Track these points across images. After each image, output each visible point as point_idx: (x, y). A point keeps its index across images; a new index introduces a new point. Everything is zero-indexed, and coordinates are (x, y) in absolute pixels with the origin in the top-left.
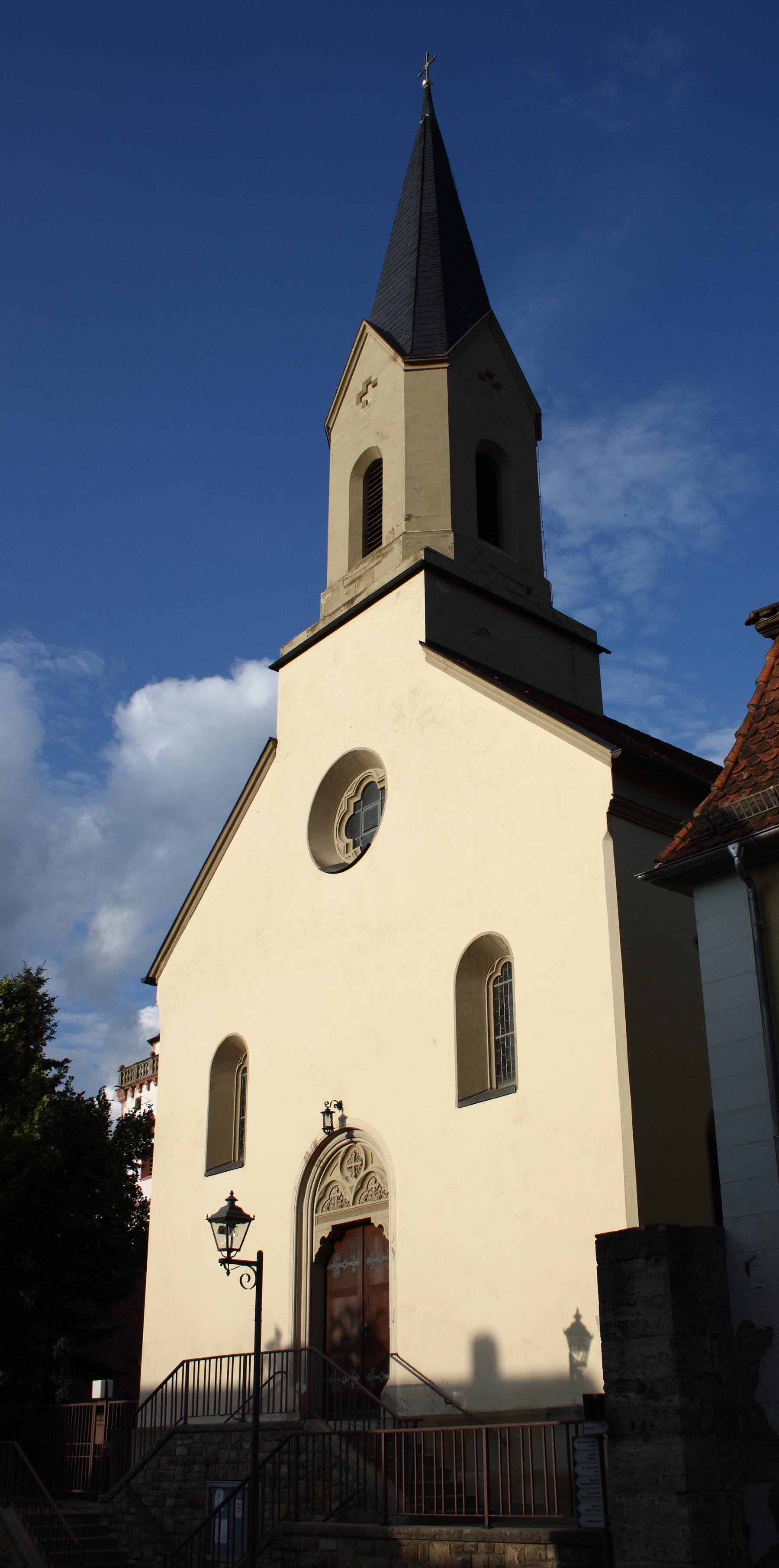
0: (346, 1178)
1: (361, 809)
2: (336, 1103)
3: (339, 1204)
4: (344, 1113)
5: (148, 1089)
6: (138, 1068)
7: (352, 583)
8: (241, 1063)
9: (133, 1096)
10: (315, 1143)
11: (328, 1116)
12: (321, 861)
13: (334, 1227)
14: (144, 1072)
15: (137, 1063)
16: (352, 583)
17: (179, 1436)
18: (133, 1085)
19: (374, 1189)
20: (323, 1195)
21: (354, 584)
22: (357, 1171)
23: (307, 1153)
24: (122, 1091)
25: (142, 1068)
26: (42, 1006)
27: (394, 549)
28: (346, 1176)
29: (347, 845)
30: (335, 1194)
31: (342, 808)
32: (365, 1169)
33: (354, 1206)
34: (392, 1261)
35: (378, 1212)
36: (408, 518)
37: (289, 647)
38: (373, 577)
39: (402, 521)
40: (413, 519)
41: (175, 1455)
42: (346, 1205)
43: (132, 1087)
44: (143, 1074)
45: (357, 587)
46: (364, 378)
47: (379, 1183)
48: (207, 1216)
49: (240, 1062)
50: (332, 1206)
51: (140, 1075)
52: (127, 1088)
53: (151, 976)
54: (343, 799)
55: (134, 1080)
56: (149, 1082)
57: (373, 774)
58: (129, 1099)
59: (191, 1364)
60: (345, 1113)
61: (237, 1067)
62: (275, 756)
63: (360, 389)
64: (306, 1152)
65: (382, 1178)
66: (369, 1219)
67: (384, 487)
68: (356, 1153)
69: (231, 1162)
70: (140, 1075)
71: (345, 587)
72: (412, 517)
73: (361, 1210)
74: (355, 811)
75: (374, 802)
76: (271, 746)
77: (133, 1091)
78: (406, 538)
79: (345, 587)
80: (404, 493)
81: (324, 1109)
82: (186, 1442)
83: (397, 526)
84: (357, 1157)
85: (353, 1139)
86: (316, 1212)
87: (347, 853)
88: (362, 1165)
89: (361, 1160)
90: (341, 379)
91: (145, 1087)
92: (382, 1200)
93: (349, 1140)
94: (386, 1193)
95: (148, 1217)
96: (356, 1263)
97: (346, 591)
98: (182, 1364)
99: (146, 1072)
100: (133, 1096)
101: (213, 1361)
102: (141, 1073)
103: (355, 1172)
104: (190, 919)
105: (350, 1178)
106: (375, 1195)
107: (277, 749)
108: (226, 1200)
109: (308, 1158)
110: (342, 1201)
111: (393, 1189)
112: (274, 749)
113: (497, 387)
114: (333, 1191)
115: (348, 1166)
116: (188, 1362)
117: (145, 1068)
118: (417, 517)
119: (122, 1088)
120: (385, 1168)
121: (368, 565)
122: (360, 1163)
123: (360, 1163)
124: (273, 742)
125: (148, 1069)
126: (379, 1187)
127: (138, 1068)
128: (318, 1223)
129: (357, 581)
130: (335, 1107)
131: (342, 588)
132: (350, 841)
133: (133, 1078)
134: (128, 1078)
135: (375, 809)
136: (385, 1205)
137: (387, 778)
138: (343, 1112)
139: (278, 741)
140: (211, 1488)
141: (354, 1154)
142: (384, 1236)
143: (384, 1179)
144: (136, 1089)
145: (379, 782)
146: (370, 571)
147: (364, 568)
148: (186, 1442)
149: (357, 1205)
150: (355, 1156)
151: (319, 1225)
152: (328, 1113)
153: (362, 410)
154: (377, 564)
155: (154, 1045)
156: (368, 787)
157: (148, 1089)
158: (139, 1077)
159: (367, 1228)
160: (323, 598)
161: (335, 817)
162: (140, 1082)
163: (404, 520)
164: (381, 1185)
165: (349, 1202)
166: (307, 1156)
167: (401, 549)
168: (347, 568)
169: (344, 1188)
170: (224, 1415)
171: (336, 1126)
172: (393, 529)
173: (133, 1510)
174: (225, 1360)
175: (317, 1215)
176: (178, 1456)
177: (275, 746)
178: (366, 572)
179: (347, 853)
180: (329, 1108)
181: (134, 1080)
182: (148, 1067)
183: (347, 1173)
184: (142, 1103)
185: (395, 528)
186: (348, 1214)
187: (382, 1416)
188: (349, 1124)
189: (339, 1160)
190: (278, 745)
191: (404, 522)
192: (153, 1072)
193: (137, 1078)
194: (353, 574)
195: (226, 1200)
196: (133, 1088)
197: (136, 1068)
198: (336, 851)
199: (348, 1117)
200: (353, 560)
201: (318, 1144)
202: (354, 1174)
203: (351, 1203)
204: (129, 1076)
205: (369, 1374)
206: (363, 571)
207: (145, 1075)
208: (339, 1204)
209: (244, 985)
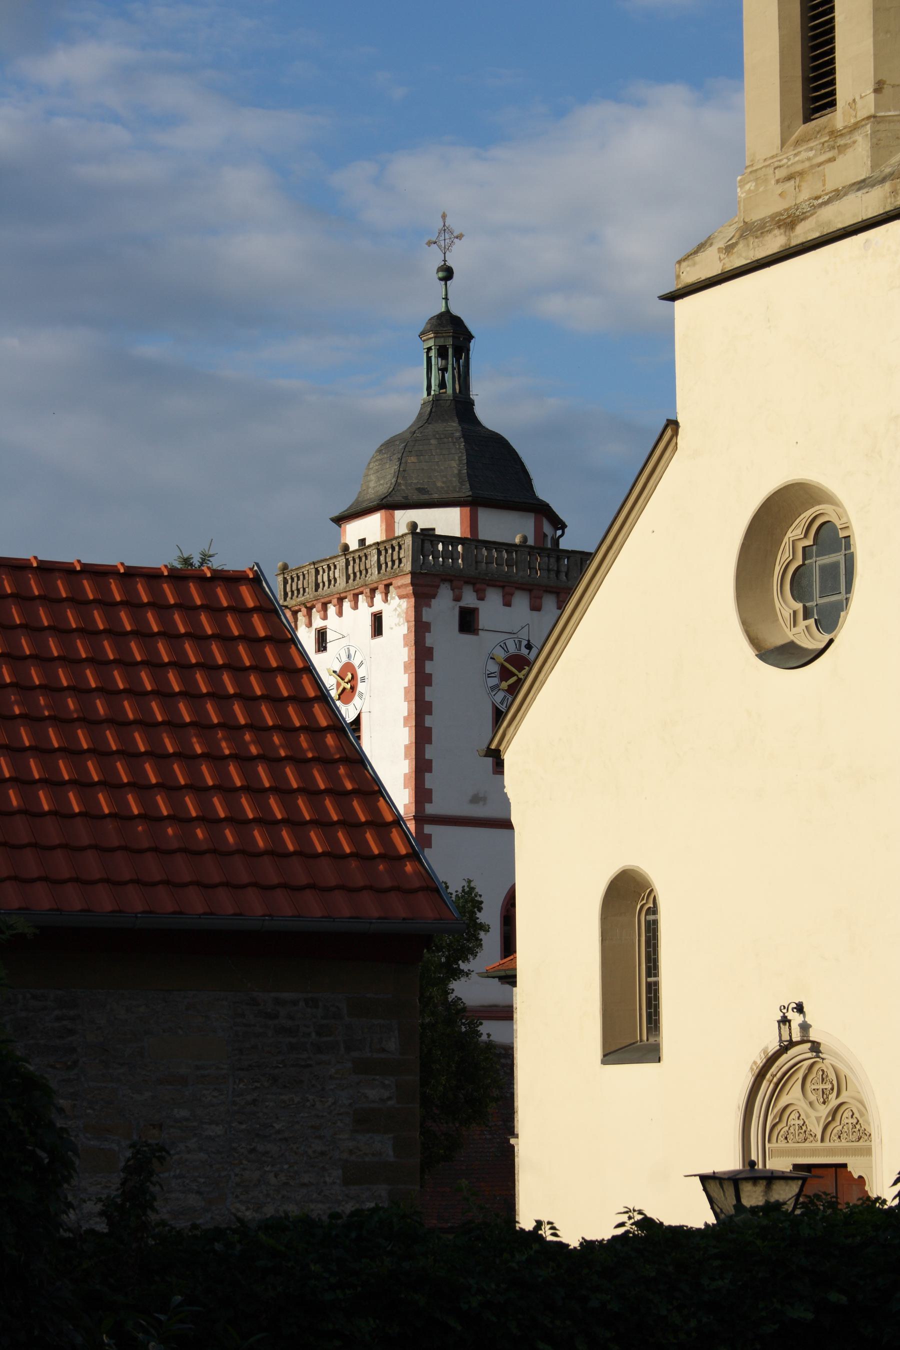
0: (811, 1104)
1: (814, 559)
2: (795, 1006)
3: (801, 1135)
4: (806, 1020)
5: (340, 613)
6: (317, 572)
7: (789, 178)
8: (644, 901)
9: (310, 624)
10: (765, 1051)
11: (785, 1024)
12: (757, 639)
14: (330, 581)
15: (314, 563)
16: (789, 178)
18: (308, 605)
19: (851, 1126)
20: (777, 1120)
21: (792, 182)
22: (825, 1096)
23: (755, 1063)
25: (324, 572)
26: (192, 567)
27: (856, 144)
28: (811, 1100)
29: (795, 612)
30: (794, 1121)
31: (784, 555)
33: (823, 1144)
35: (856, 1158)
36: (879, 88)
37: (688, 266)
38: (824, 181)
39: (868, 92)
40: (887, 90)
42: (812, 1139)
43: (306, 607)
44: (327, 584)
45: (797, 189)
47: (856, 1118)
49: (643, 899)
50: (792, 1137)
51: (321, 585)
52: (296, 608)
53: (493, 747)
54: (786, 539)
55: (310, 594)
56: (341, 600)
57: (829, 513)
60: (809, 1020)
61: (639, 907)
64: (752, 1062)
65: (862, 1115)
67: (839, 54)
68: (823, 1071)
69: (637, 1042)
70: (321, 585)
71: (778, 181)
72: (885, 86)
73: (831, 1152)
74: (804, 558)
75: (834, 553)
76: (669, 433)
77: (309, 615)
78: (876, 129)
79: (778, 181)
80: (871, 40)
81: (779, 1016)
83: (861, 97)
84: (824, 1076)
85: (820, 1054)
86: (769, 1141)
87: (794, 626)
88: (832, 1089)
89: (831, 1083)
90: (845, 545)
91: (332, 610)
92: (861, 1143)
93: (814, 1054)
94: (868, 1134)
95: (603, 1240)
97: (779, 189)
99: (332, 581)
100: (310, 624)
102: (324, 583)
103: (823, 1097)
104: (550, 673)
105: (816, 1104)
106: (852, 1134)
107: (679, 437)
110: (805, 1132)
111: (878, 1138)
112: (675, 437)
114: (792, 1116)
115: (814, 1087)
117: (331, 572)
118: (893, 86)
120: (865, 1100)
121: (815, 156)
122: (829, 1086)
123: (830, 1086)
124: (673, 425)
125: (337, 575)
126: (857, 1124)
127: (317, 572)
128: (771, 1157)
129: (798, 179)
130: (793, 1011)
131: (773, 182)
132: (799, 606)
133: (307, 589)
134: (298, 590)
135: (840, 602)
136: (868, 1152)
137: (854, 534)
138: (804, 1017)
139: (680, 424)
141: (821, 1073)
142: (867, 1191)
143: (864, 1115)
144: (314, 610)
145: (840, 529)
146: (818, 169)
147: (809, 159)
149: (827, 1144)
150: (822, 1075)
151: (773, 1159)
152: (784, 1021)
155: (342, 526)
156: (824, 526)
157: (340, 613)
158: (320, 589)
159: (842, 1169)
160: (741, 187)
161: (775, 565)
162: (323, 600)
163: (872, 90)
164: (860, 1122)
165: (815, 1136)
167: (868, 148)
168: (779, 142)
169: (808, 1116)
171: (796, 1037)
172: (854, 100)
175: (771, 1145)
177: (676, 433)
178: (812, 167)
179: (794, 626)
180: (786, 1015)
181: (310, 594)
182: (337, 571)
183: (812, 1097)
184: (329, 638)
186: (814, 1152)
188: (813, 1035)
189: (800, 1075)
190: (680, 430)
191: (873, 95)
192: (347, 582)
193: (316, 590)
194: (790, 163)
196: (309, 610)
197: (313, 571)
198: (778, 620)
199: (813, 1027)
200: (789, 127)
201: (770, 1054)
202: (822, 1100)
203: (819, 1136)
204: (300, 586)
206: (807, 164)
207: (332, 586)
208: (801, 1135)
209: (646, 798)
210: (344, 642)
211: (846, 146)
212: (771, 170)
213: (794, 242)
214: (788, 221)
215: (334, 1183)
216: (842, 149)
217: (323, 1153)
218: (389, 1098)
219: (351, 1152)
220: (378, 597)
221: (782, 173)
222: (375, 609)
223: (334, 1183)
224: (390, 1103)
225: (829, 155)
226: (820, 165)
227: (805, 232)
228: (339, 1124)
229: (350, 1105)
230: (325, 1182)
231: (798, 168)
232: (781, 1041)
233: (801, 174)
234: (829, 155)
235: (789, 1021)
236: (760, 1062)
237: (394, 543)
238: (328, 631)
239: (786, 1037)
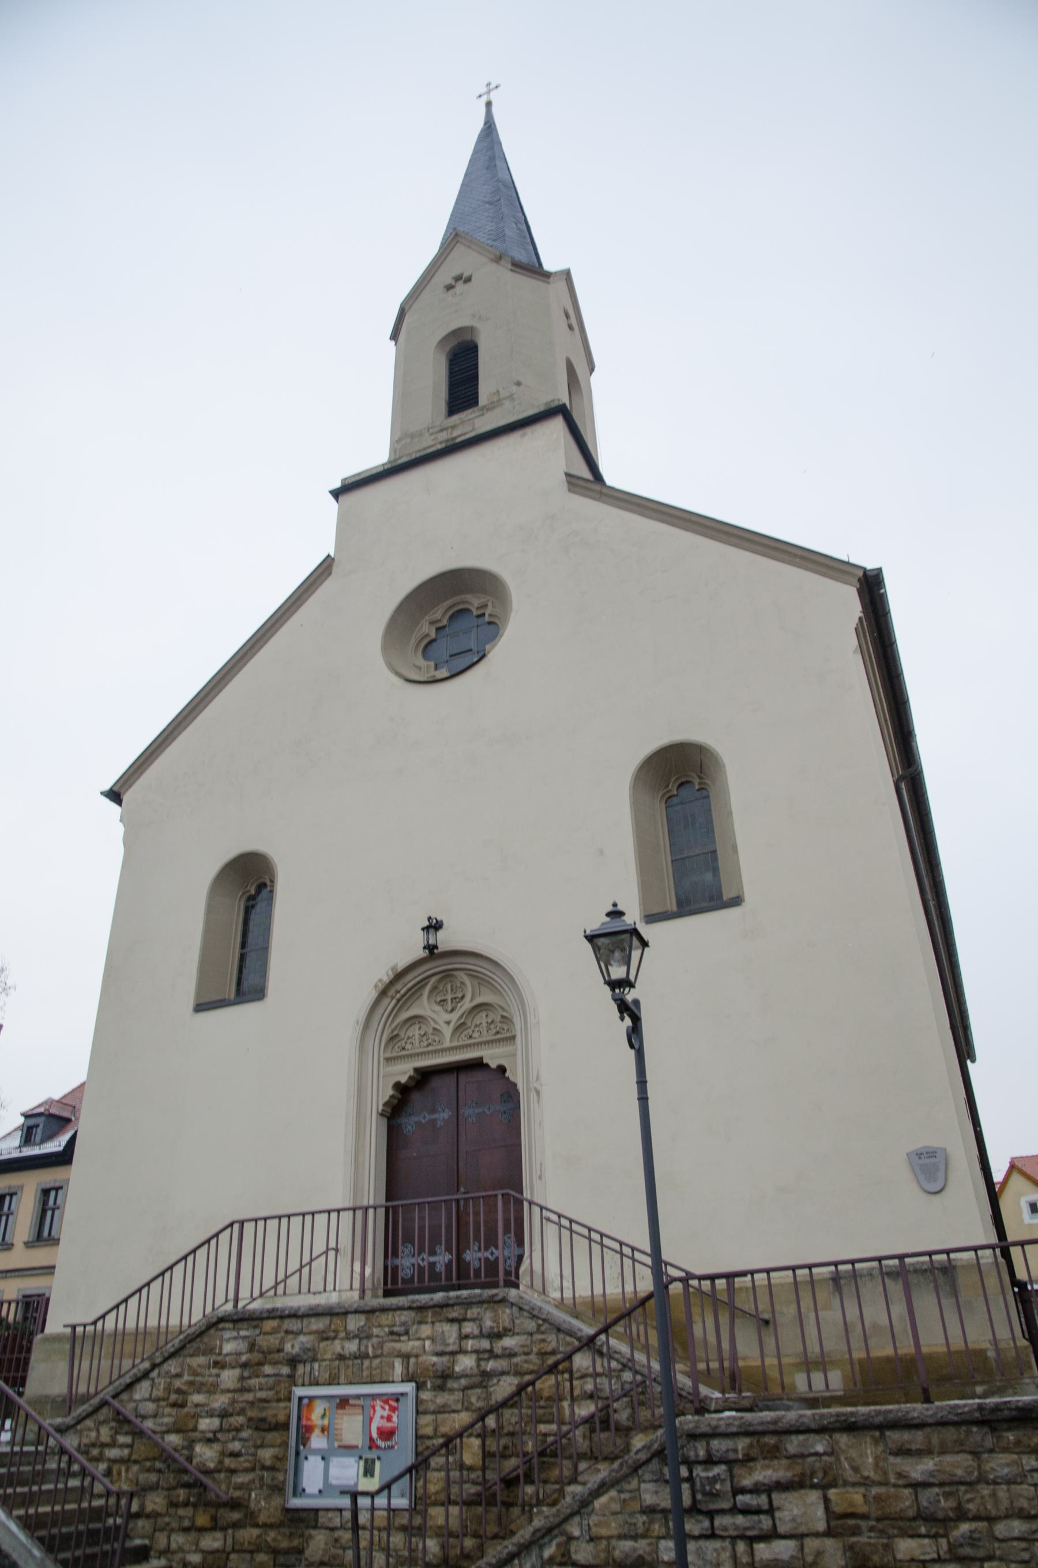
13: (416, 1070)
17: (230, 1325)
23: (380, 980)
32: (472, 1000)
34: (536, 1105)
41: (220, 1354)
46: (456, 272)
48: (585, 932)
59: (249, 1227)
63: (450, 281)
66: (481, 1058)
82: (243, 1333)
96: (444, 1115)
98: (231, 1225)
101: (273, 1224)
108: (22, 1114)
109: (381, 986)
116: (242, 1223)
140: (300, 1399)
148: (243, 1333)
154: (478, 416)
166: (380, 985)
170: (320, 1293)
173: (122, 1439)
174: (296, 1221)
176: (227, 1355)
185: (501, 390)
195: (22, 1114)
205: (468, 1251)
236: (386, 980)
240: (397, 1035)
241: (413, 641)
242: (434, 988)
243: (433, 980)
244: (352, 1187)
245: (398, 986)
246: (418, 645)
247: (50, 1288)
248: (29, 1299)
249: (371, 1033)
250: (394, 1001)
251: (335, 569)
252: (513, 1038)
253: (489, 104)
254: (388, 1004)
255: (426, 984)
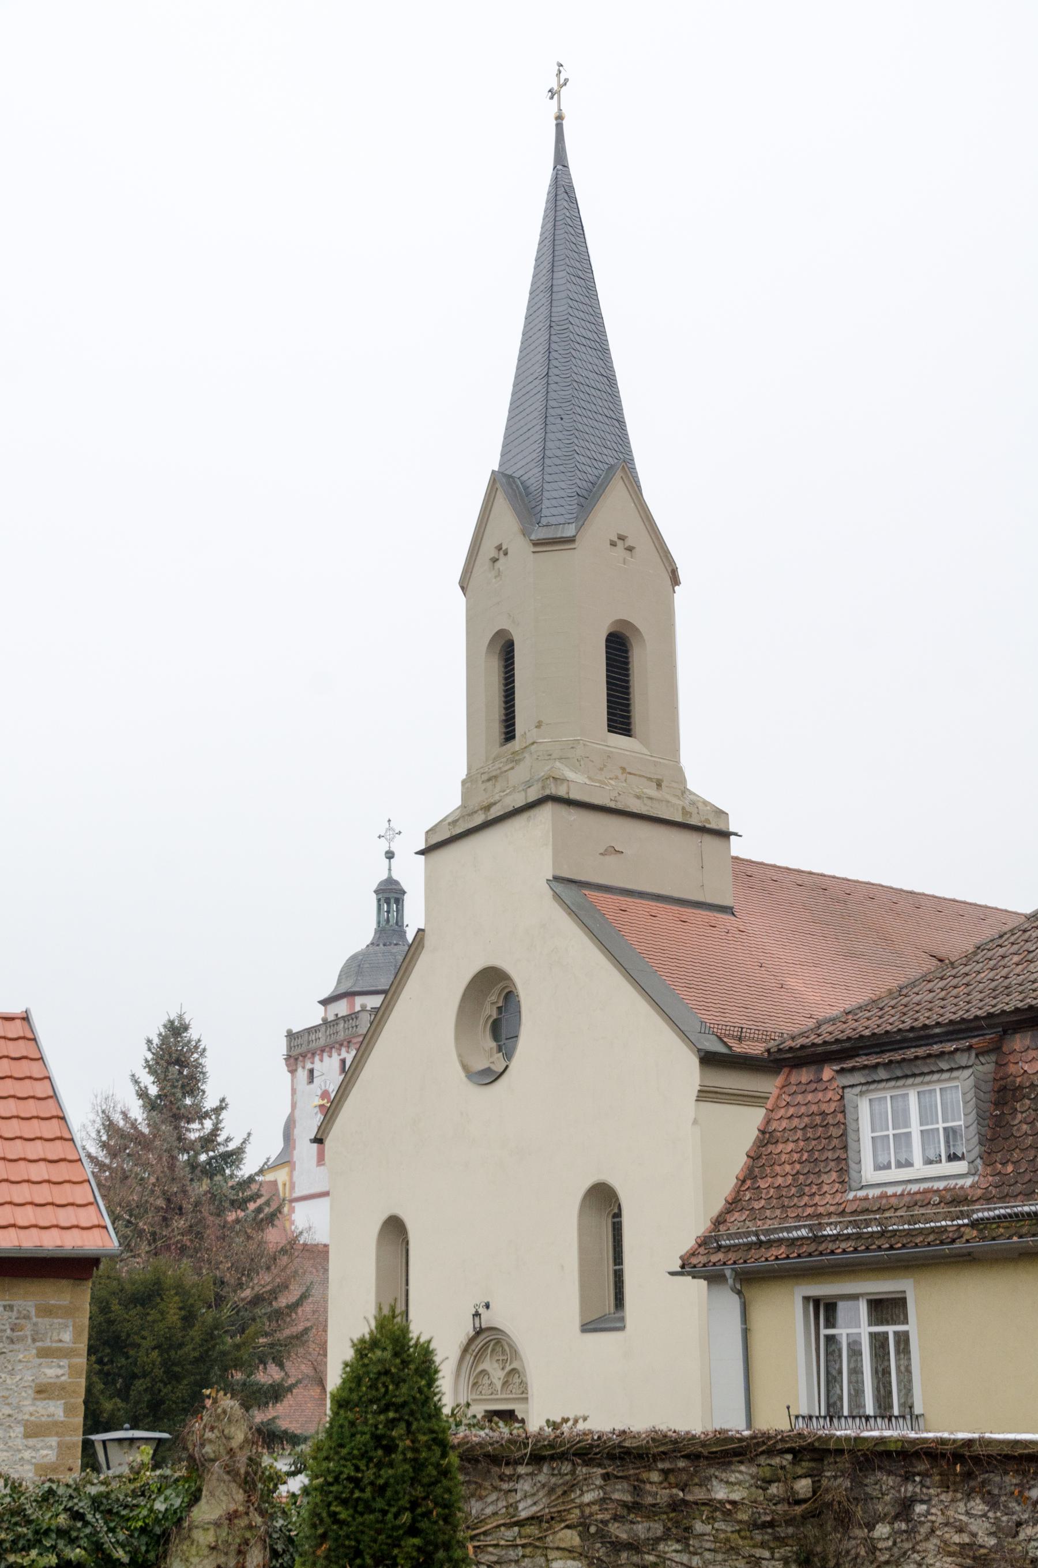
5: (321, 1060)
7: (489, 780)
9: (304, 1068)
13: (486, 1411)
16: (489, 780)
24: (292, 1060)
58: (300, 1070)
62: (423, 947)
71: (483, 782)
79: (483, 782)
100: (304, 1068)
109: (462, 1348)
113: (630, 549)
119: (290, 1056)
147: (500, 768)
152: (477, 1314)
153: (494, 580)
157: (321, 1060)
178: (502, 773)
187: (1025, 1203)
206: (498, 771)
210: (323, 1077)
211: (520, 760)
212: (479, 775)
213: (489, 818)
214: (487, 808)
215: (17, 1437)
216: (518, 762)
217: (9, 1416)
218: (63, 1375)
219: (31, 1414)
220: (344, 1050)
221: (485, 777)
222: (342, 1057)
223: (17, 1437)
224: (63, 1378)
225: (511, 765)
226: (506, 771)
227: (495, 812)
228: (24, 1394)
229: (33, 1380)
230: (10, 1437)
231: (494, 774)
232: (474, 1328)
233: (496, 777)
234: (511, 765)
235: (480, 1315)
236: (465, 1342)
237: (353, 1016)
238: (315, 1071)
239: (477, 1325)
240: (477, 1382)
241: (482, 1022)
242: (493, 1350)
243: (492, 1343)
244: (893, 1296)
245: (473, 1347)
246: (485, 1027)
247: (527, 1412)
248: (837, 1354)
249: (462, 1379)
250: (472, 1358)
251: (427, 943)
252: (624, 1327)
253: (559, 118)
254: (470, 1359)
255: (488, 1347)
